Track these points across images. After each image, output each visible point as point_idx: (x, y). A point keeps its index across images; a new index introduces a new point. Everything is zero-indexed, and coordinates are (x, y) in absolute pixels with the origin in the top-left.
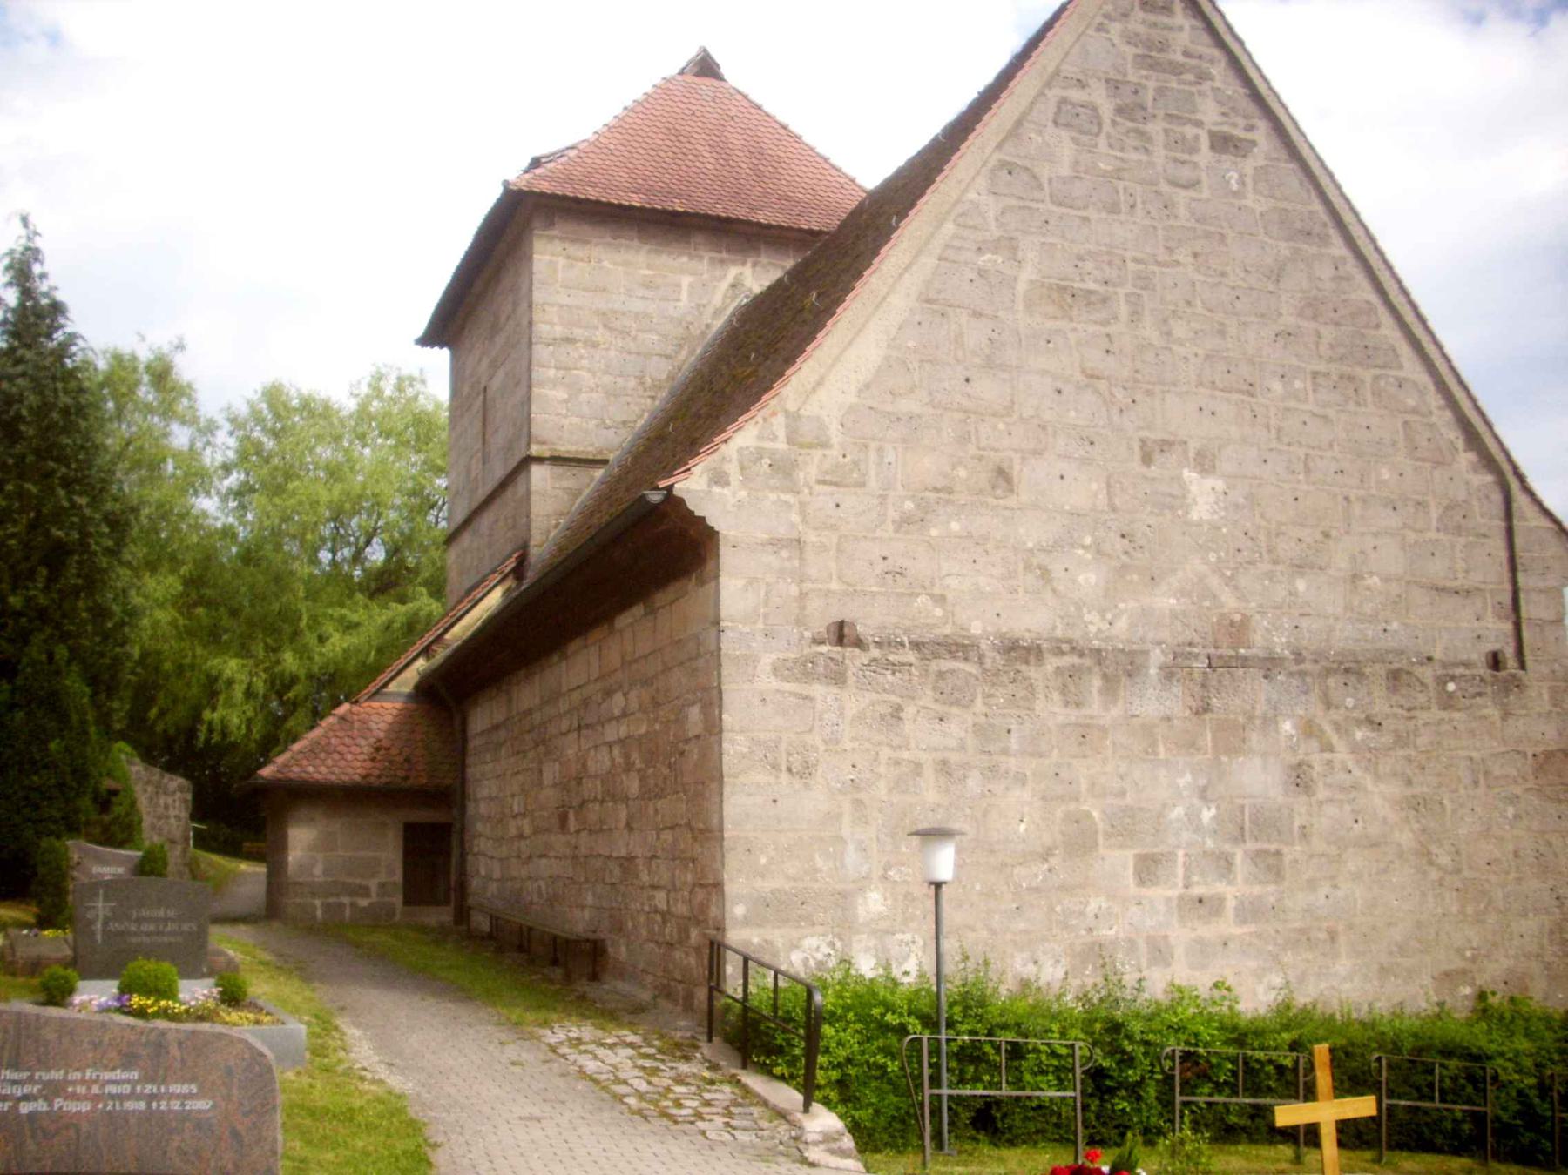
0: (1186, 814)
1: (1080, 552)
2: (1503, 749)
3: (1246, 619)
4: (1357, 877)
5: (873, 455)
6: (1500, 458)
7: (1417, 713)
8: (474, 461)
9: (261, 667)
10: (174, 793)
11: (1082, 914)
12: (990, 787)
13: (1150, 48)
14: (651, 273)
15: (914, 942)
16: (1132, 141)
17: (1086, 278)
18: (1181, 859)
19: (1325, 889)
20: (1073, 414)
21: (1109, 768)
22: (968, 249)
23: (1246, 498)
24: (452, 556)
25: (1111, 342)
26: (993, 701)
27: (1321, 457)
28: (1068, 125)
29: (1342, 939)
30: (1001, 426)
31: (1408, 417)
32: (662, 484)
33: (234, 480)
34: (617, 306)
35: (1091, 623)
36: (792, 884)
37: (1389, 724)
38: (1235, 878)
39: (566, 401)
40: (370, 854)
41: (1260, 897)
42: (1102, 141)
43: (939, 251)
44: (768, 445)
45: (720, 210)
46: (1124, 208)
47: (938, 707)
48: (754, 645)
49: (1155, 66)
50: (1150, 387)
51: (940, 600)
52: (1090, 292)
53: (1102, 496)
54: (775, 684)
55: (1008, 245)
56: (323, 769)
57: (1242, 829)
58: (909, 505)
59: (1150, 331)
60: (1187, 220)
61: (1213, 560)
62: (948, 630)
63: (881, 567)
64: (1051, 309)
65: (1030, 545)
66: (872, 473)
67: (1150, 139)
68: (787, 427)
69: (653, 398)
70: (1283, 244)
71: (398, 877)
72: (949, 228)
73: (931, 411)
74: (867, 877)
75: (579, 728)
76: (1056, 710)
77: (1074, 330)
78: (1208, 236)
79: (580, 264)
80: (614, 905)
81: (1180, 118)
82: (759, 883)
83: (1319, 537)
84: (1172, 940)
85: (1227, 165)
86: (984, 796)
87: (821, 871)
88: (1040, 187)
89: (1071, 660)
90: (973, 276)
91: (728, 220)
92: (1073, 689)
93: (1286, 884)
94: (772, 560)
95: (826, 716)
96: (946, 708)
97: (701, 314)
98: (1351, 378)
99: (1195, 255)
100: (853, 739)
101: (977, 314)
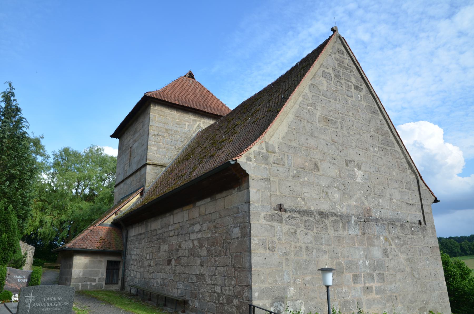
0: (363, 263)
1: (334, 188)
2: (425, 246)
3: (370, 209)
4: (400, 280)
5: (286, 157)
6: (416, 171)
7: (407, 236)
8: (126, 165)
9: (55, 218)
10: (30, 250)
11: (342, 292)
12: (318, 254)
13: (340, 63)
14: (179, 121)
15: (302, 303)
16: (338, 84)
17: (331, 116)
18: (362, 276)
19: (394, 284)
20: (330, 151)
21: (345, 250)
22: (305, 105)
23: (368, 177)
24: (116, 190)
25: (337, 133)
26: (318, 229)
27: (382, 168)
28: (325, 77)
29: (398, 298)
30: (315, 152)
31: (397, 160)
32: (234, 159)
33: (52, 171)
34: (170, 128)
35: (338, 208)
36: (270, 285)
37: (402, 238)
38: (374, 281)
39: (157, 150)
40: (97, 269)
41: (380, 287)
42: (332, 82)
43: (299, 104)
44: (262, 151)
45: (196, 107)
46: (338, 100)
47: (305, 230)
48: (259, 210)
49: (341, 67)
50: (346, 146)
51: (303, 199)
52: (332, 120)
53: (338, 174)
54: (264, 222)
55: (313, 105)
56: (86, 245)
57: (375, 267)
58: (295, 172)
59: (345, 132)
60: (351, 105)
61: (362, 193)
62: (305, 208)
63: (289, 189)
64: (324, 123)
65: (323, 185)
66: (286, 162)
67: (342, 84)
68: (266, 146)
69: (178, 151)
70: (370, 114)
71: (104, 276)
72: (301, 98)
73: (299, 146)
74: (290, 283)
75: (178, 235)
76: (332, 232)
77: (329, 129)
78: (355, 110)
79: (162, 117)
80: (193, 289)
81: (348, 80)
82: (261, 285)
83: (383, 188)
84: (363, 300)
85: (358, 93)
86: (317, 257)
87: (278, 281)
88: (320, 91)
89: (335, 218)
90: (307, 112)
91: (198, 110)
92: (335, 226)
93: (385, 282)
94: (263, 184)
95: (278, 232)
96: (307, 231)
97: (190, 132)
98: (386, 149)
99: (353, 114)
100: (285, 240)
101: (308, 122)
